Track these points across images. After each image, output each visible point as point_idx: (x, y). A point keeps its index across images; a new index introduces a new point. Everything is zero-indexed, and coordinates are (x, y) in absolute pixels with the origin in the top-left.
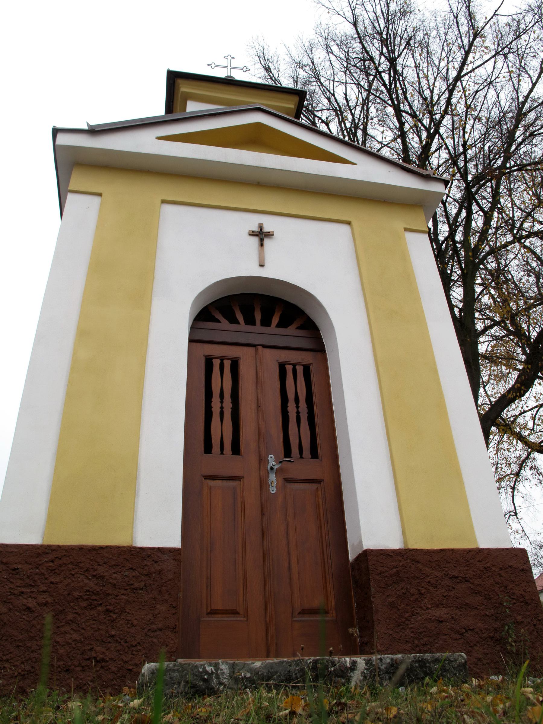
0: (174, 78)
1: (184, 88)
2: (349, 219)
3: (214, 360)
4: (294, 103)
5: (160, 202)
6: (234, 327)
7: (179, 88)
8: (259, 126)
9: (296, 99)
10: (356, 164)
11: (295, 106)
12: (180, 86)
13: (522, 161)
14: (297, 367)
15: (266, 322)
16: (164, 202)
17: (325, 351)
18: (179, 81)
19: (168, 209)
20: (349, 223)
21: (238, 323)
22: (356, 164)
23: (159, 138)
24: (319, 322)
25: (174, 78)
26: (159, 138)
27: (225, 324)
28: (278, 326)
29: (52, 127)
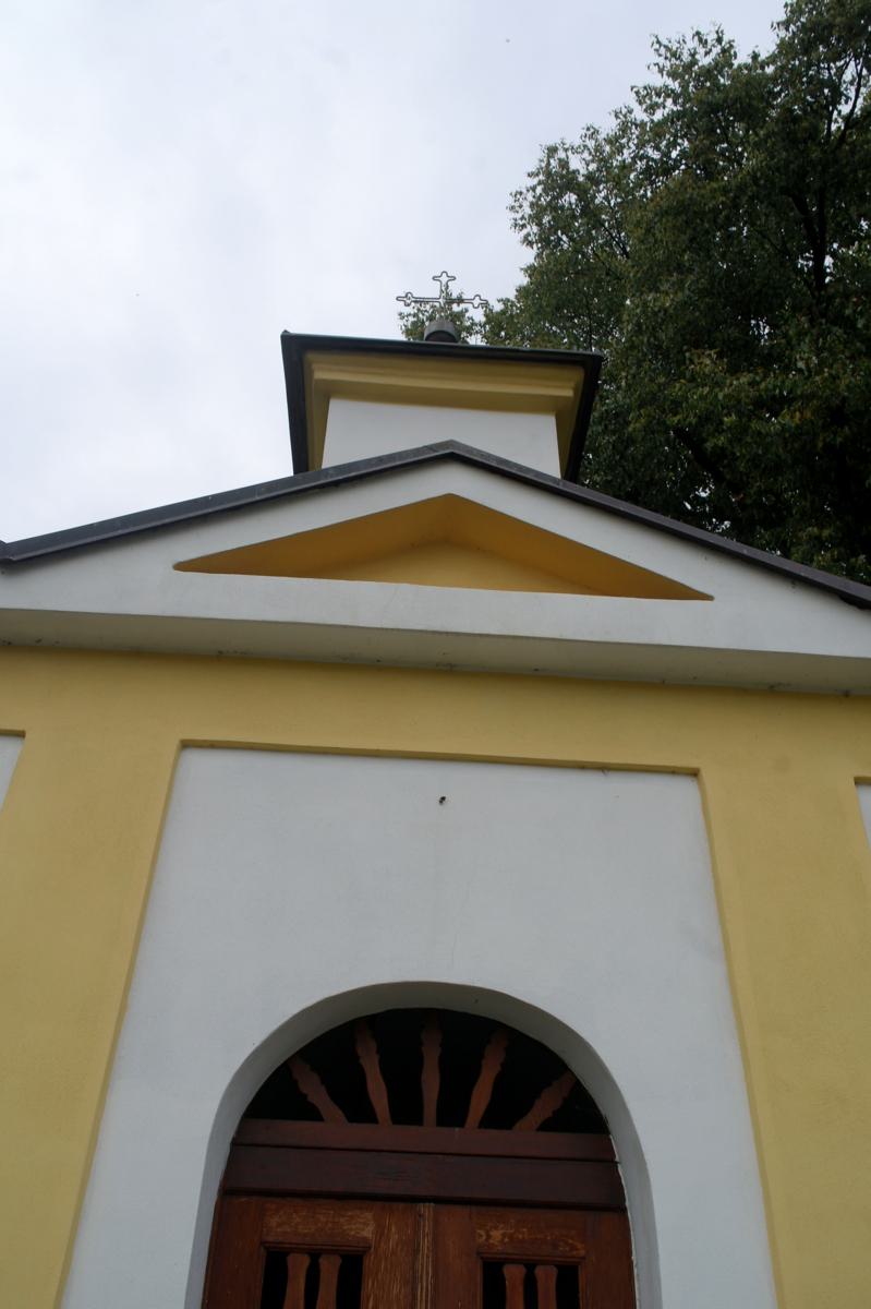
0: (299, 351)
1: (323, 371)
2: (692, 763)
3: (291, 1259)
4: (572, 384)
5: (174, 744)
6: (359, 1133)
7: (312, 372)
8: (451, 501)
9: (576, 376)
10: (709, 598)
11: (575, 390)
12: (314, 366)
13: (818, 72)
14: (539, 1271)
15: (452, 1113)
16: (186, 745)
17: (624, 1210)
18: (311, 356)
19: (197, 761)
20: (694, 773)
21: (370, 1117)
22: (709, 598)
23: (182, 567)
24: (605, 1108)
25: (299, 351)
26: (182, 567)
27: (335, 1127)
28: (489, 1121)
29: (534, 159)
